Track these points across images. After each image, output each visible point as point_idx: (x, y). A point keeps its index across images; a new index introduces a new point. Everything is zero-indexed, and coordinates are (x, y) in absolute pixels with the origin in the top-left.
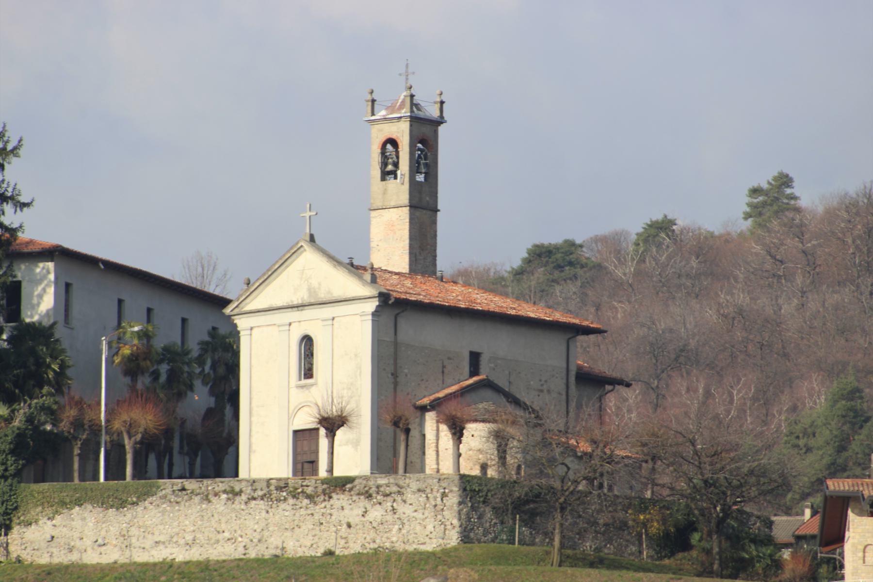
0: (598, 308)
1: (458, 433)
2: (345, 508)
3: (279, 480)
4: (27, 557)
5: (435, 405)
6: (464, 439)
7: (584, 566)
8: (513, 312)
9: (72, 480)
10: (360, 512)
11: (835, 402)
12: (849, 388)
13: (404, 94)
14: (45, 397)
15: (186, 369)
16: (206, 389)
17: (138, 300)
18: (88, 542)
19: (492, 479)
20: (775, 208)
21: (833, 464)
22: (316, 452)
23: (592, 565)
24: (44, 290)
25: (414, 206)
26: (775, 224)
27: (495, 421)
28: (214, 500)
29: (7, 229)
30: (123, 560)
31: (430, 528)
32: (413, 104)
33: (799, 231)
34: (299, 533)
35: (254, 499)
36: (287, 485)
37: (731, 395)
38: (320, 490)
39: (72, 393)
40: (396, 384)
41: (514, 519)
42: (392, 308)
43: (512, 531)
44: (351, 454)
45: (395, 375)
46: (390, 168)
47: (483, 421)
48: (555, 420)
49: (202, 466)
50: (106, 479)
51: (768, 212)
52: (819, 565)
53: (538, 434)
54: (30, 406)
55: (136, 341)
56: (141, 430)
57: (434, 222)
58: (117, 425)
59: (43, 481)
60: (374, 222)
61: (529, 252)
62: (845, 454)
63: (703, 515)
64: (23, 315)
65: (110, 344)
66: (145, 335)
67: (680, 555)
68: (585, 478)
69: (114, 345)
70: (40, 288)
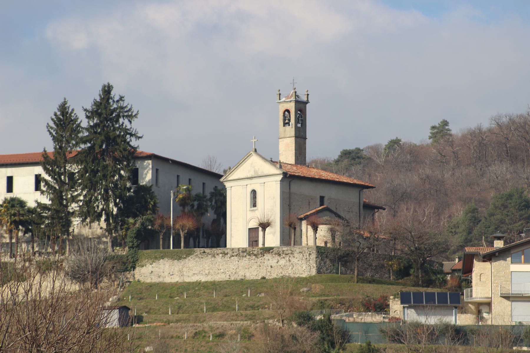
0: (370, 176)
1: (315, 229)
2: (270, 260)
3: (243, 248)
4: (142, 279)
5: (306, 218)
6: (318, 232)
7: (367, 283)
8: (337, 180)
9: (159, 248)
10: (276, 261)
11: (467, 214)
12: (472, 208)
13: (292, 91)
14: (149, 215)
15: (205, 203)
16: (213, 211)
17: (185, 175)
18: (166, 274)
19: (329, 248)
20: (441, 134)
21: (466, 239)
22: (258, 237)
23: (370, 282)
24: (148, 172)
25: (297, 137)
26: (442, 141)
27: (330, 224)
28: (217, 256)
29: (132, 147)
30: (180, 281)
31: (304, 267)
32: (296, 95)
33: (452, 144)
34: (251, 270)
35: (233, 256)
36: (246, 250)
37: (424, 211)
38: (259, 252)
39: (159, 213)
40: (290, 209)
41: (338, 264)
42: (288, 179)
43: (338, 269)
44: (272, 238)
45: (289, 206)
46: (287, 121)
47: (326, 224)
48: (355, 224)
49: (211, 243)
50: (173, 248)
51: (438, 136)
52: (462, 282)
53: (348, 230)
54: (142, 219)
55: (184, 192)
56: (187, 228)
57: (305, 143)
58: (177, 226)
59: (148, 249)
60: (280, 143)
61: (341, 153)
62: (471, 235)
63: (415, 262)
64: (139, 182)
65: (174, 194)
66: (188, 190)
67: (406, 278)
68: (367, 247)
69: (176, 194)
70: (146, 171)
